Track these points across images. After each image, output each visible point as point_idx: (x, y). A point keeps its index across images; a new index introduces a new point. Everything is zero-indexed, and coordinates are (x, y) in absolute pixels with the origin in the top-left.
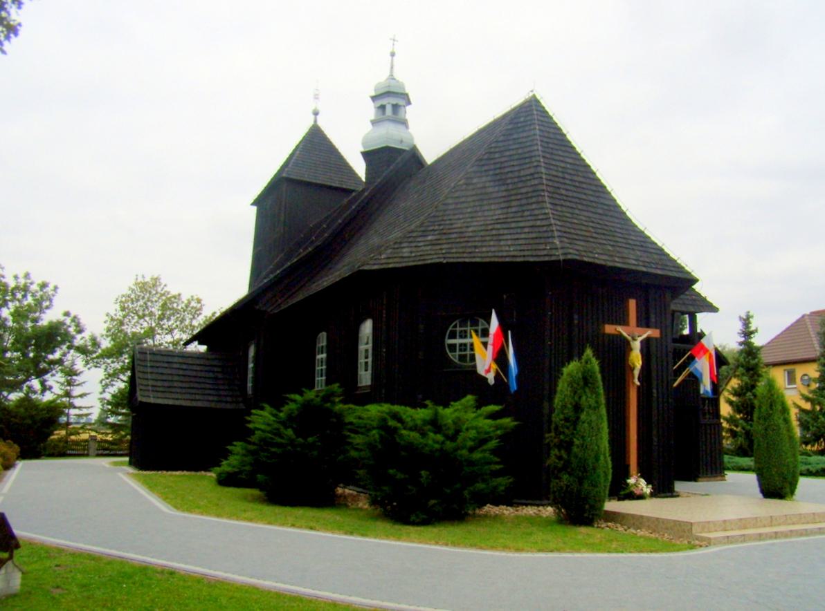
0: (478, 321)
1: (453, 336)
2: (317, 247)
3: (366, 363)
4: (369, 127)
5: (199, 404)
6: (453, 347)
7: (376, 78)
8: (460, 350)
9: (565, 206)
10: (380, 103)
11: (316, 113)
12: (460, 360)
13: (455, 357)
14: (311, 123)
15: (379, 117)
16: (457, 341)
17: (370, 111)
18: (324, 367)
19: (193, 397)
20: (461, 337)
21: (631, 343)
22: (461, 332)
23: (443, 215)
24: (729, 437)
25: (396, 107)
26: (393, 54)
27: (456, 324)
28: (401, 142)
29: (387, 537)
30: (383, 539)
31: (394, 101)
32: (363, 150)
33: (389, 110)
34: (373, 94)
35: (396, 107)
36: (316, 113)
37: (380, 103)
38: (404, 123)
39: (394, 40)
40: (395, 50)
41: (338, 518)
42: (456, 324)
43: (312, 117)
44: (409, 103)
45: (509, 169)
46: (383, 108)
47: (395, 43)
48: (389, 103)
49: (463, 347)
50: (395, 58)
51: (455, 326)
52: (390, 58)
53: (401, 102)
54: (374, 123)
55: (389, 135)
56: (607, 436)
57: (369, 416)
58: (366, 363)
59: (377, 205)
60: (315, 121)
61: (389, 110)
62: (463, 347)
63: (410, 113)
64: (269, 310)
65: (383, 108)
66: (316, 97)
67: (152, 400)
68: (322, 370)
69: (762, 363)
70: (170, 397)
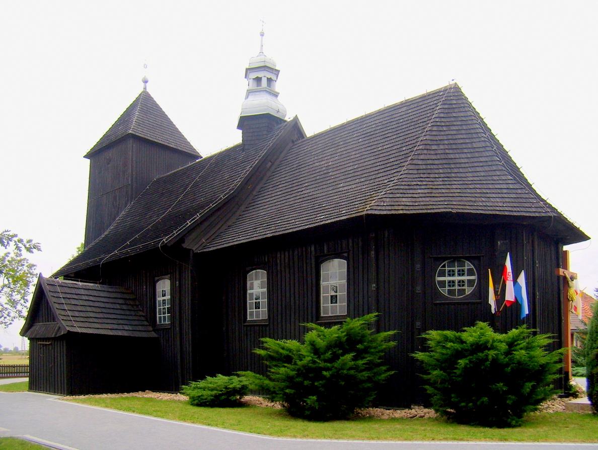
0: (465, 262)
1: (442, 274)
5: (120, 333)
6: (442, 284)
10: (254, 75)
11: (146, 82)
12: (449, 294)
13: (444, 291)
14: (140, 90)
15: (254, 88)
17: (244, 84)
19: (135, 328)
20: (449, 275)
21: (570, 282)
22: (449, 271)
26: (262, 35)
27: (445, 264)
28: (278, 112)
29: (477, 439)
30: (480, 440)
31: (269, 75)
33: (264, 82)
36: (146, 82)
37: (254, 75)
38: (276, 95)
39: (263, 22)
41: (398, 426)
42: (445, 264)
43: (143, 84)
44: (277, 72)
45: (462, 141)
46: (258, 80)
48: (265, 76)
50: (264, 37)
51: (444, 266)
53: (274, 78)
54: (250, 92)
55: (260, 104)
59: (270, 164)
60: (145, 88)
61: (264, 82)
63: (278, 86)
64: (194, 249)
65: (258, 80)
67: (79, 330)
70: (296, 332)
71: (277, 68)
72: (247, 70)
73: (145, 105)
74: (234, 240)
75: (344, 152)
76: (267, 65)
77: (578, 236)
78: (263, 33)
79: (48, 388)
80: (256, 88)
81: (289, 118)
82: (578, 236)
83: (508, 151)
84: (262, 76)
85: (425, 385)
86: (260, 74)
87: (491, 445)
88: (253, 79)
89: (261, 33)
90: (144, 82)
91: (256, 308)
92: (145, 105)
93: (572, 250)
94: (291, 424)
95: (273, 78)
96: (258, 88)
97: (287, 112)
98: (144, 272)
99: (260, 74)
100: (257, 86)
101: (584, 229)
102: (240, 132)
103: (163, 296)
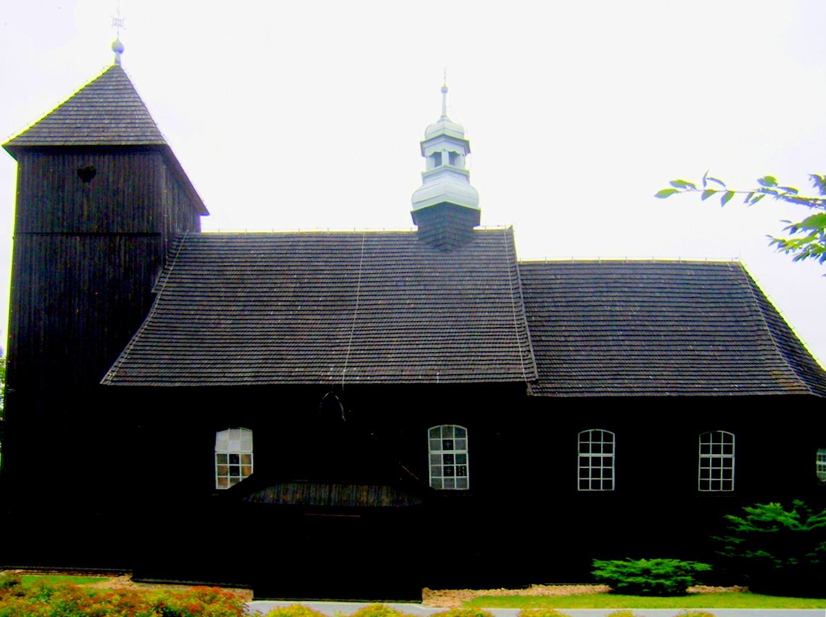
7: (424, 122)
8: (451, 448)
11: (119, 50)
14: (111, 63)
15: (432, 169)
16: (711, 456)
17: (423, 164)
23: (104, 86)
24: (820, 250)
25: (453, 156)
26: (444, 91)
32: (413, 210)
33: (445, 159)
34: (424, 140)
36: (119, 50)
37: (429, 152)
38: (466, 175)
40: (448, 85)
43: (114, 55)
44: (466, 145)
46: (437, 156)
48: (444, 150)
49: (448, 444)
50: (447, 94)
52: (442, 95)
53: (459, 150)
54: (426, 177)
55: (447, 189)
57: (92, 592)
60: (118, 61)
61: (445, 159)
62: (448, 444)
63: (469, 162)
65: (437, 156)
66: (118, 23)
71: (466, 138)
72: (422, 143)
73: (112, 88)
75: (485, 274)
77: (206, 213)
78: (446, 88)
81: (487, 223)
82: (206, 213)
84: (446, 150)
85: (746, 507)
90: (115, 51)
91: (458, 475)
92: (112, 88)
95: (458, 152)
96: (439, 167)
98: (41, 350)
99: (438, 148)
100: (436, 166)
101: (210, 212)
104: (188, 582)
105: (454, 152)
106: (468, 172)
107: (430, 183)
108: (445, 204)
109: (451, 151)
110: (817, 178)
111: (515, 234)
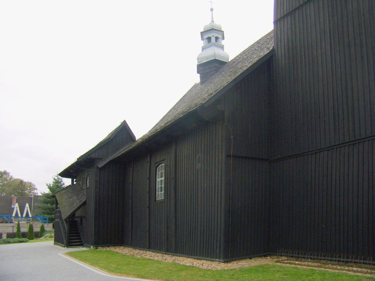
2: (61, 177)
3: (161, 187)
4: (200, 51)
9: (212, 154)
17: (202, 43)
18: (163, 178)
25: (217, 38)
26: (212, 10)
33: (213, 40)
34: (203, 30)
35: (217, 38)
37: (206, 36)
38: (222, 47)
39: (211, 2)
44: (223, 38)
46: (209, 39)
47: (212, 3)
48: (213, 36)
52: (211, 12)
54: (203, 49)
56: (253, 260)
58: (161, 187)
65: (209, 39)
68: (161, 181)
69: (51, 237)
71: (222, 30)
74: (208, 156)
76: (214, 28)
78: (213, 9)
79: (189, 253)
80: (208, 44)
83: (214, 58)
86: (210, 35)
87: (118, 278)
88: (206, 39)
89: (211, 9)
93: (197, 83)
94: (137, 252)
95: (210, 36)
97: (229, 57)
102: (199, 75)
103: (162, 172)
104: (131, 188)
105: (217, 37)
106: (223, 46)
107: (204, 51)
108: (215, 59)
109: (216, 36)
110: (212, 35)
111: (127, 122)
